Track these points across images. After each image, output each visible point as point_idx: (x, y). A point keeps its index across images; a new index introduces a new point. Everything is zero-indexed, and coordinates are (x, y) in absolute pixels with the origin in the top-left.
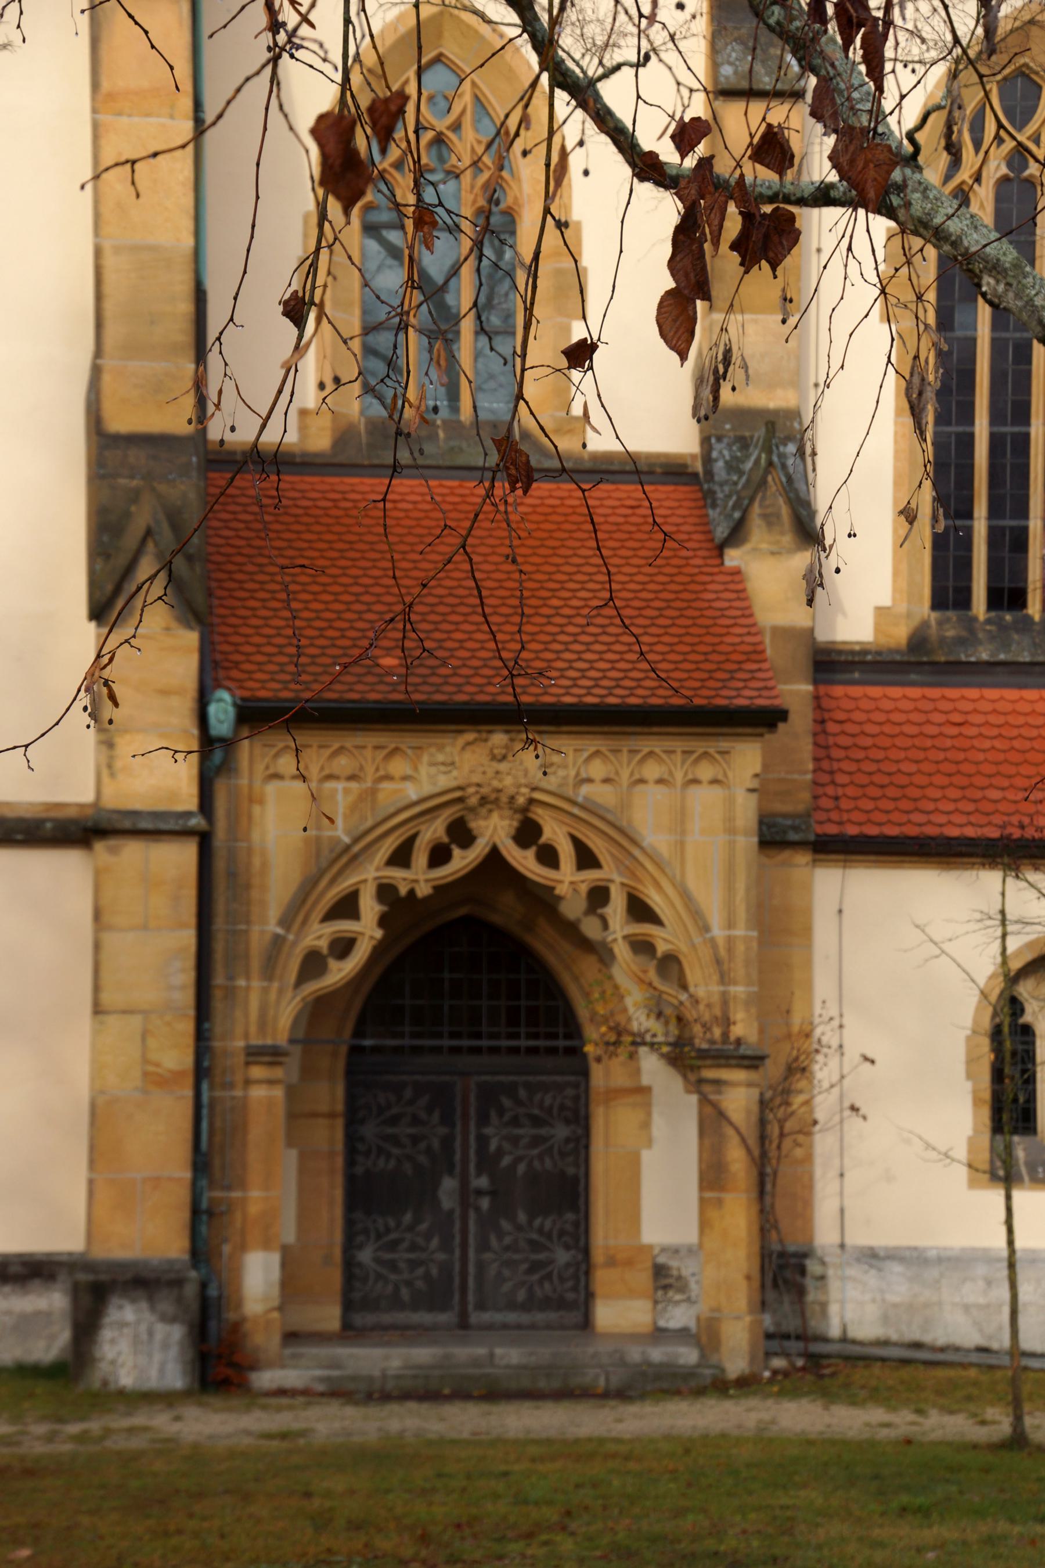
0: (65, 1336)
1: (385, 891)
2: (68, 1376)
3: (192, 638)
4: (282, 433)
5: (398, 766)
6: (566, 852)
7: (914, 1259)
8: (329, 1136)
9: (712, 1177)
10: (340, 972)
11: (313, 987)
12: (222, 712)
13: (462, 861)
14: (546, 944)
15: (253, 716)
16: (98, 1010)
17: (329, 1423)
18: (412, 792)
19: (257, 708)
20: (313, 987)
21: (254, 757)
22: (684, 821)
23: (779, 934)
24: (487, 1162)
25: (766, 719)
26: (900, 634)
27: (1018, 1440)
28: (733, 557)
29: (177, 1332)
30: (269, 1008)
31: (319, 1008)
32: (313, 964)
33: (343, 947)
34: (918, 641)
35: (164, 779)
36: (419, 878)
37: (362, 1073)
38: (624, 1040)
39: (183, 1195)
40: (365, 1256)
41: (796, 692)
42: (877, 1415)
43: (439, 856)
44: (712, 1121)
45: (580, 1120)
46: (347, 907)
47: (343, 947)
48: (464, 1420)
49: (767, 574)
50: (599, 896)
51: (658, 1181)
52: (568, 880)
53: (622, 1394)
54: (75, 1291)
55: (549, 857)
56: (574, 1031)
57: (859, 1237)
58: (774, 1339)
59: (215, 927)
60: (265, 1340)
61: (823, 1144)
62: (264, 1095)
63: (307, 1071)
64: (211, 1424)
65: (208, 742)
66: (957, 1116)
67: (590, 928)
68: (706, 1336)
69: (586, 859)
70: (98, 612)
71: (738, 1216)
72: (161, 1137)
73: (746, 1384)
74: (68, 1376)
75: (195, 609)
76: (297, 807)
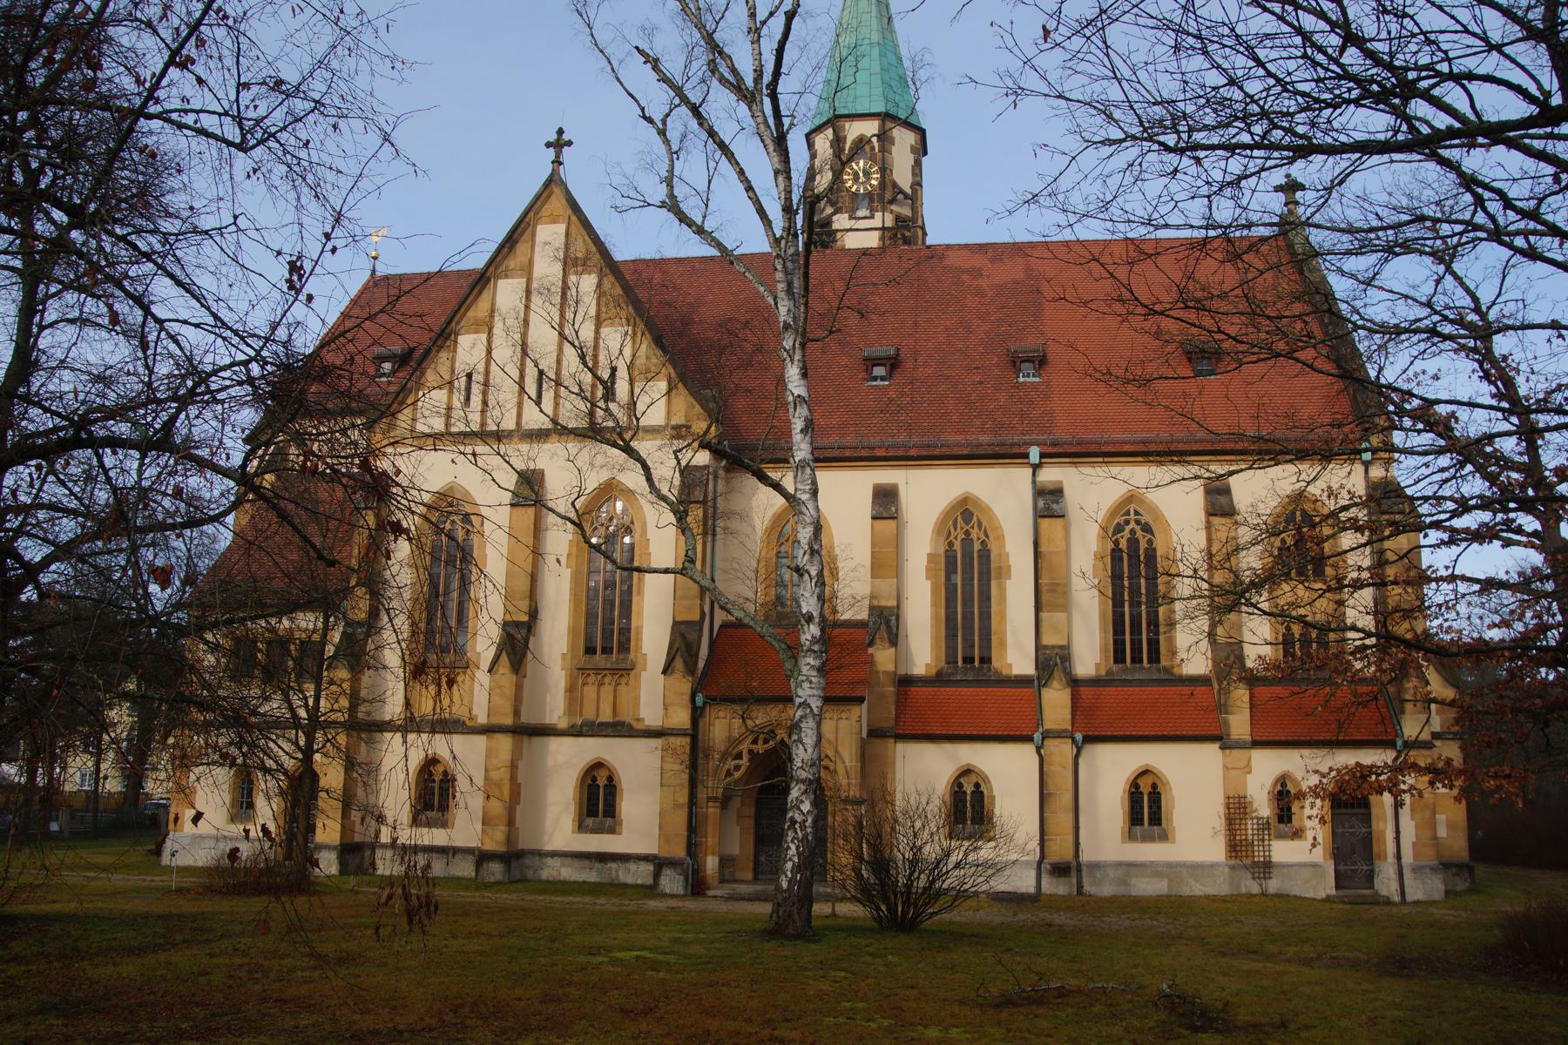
1: (750, 752)
2: (652, 890)
10: (737, 775)
12: (700, 699)
26: (933, 672)
28: (870, 650)
29: (682, 878)
33: (737, 768)
34: (939, 674)
35: (681, 718)
36: (760, 748)
39: (684, 839)
43: (766, 741)
47: (737, 768)
49: (883, 657)
64: (691, 905)
70: (664, 672)
72: (681, 818)
76: (722, 726)
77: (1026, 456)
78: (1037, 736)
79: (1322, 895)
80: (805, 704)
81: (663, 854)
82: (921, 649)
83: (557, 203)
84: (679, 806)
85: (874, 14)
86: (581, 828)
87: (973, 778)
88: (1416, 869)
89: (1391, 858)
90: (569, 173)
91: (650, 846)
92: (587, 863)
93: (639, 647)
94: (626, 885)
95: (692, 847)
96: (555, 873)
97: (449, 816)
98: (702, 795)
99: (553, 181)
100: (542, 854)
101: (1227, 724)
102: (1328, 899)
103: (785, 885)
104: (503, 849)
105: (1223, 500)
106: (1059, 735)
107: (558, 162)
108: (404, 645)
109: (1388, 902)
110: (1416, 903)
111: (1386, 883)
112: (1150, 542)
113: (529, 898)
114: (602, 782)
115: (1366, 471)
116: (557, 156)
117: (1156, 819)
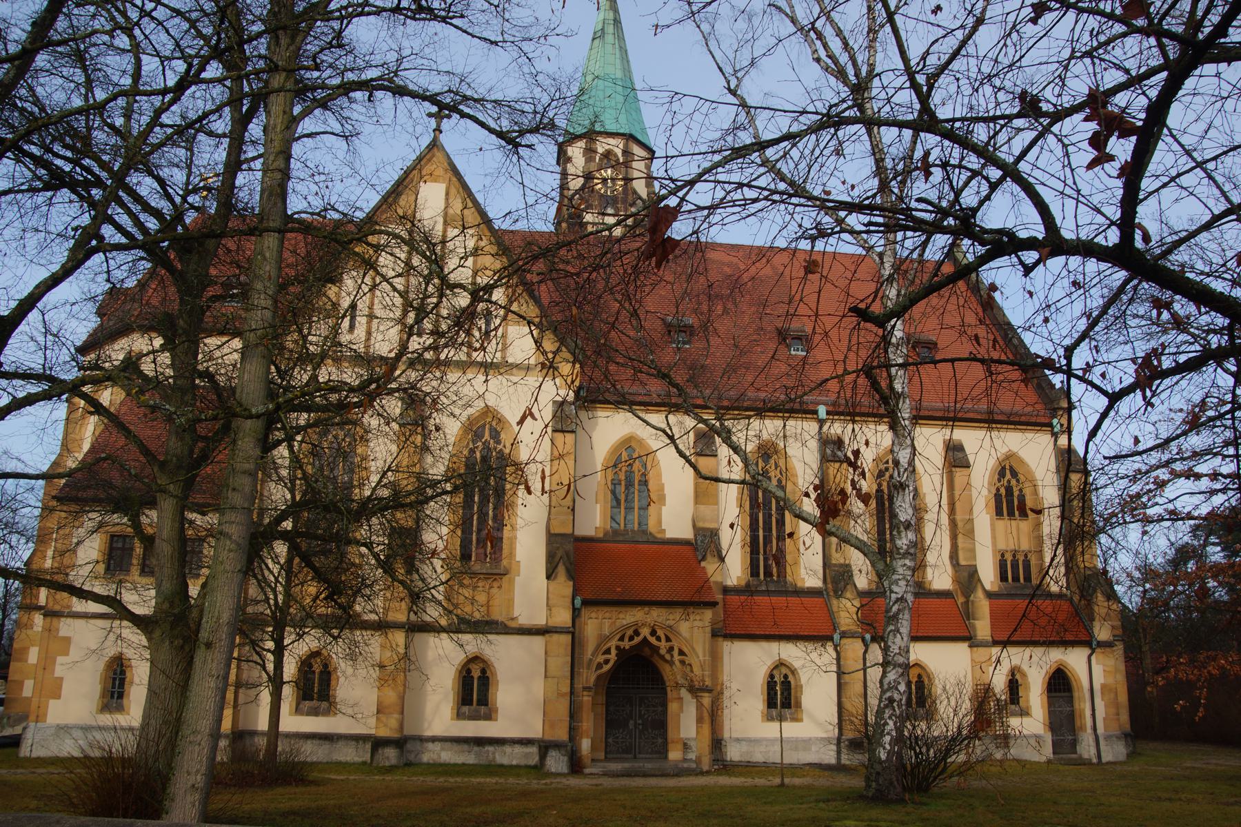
0: (537, 758)
1: (618, 648)
2: (538, 769)
3: (571, 583)
4: (590, 532)
5: (621, 616)
6: (663, 638)
7: (750, 741)
8: (602, 710)
9: (700, 720)
10: (606, 668)
11: (599, 672)
12: (578, 601)
13: (637, 640)
14: (656, 660)
15: (585, 603)
16: (546, 677)
17: (607, 782)
18: (625, 622)
19: (588, 599)
20: (599, 672)
21: (585, 613)
22: (692, 631)
23: (715, 658)
24: (641, 717)
25: (713, 604)
26: (743, 583)
27: (782, 785)
28: (703, 564)
29: (566, 758)
30: (588, 677)
31: (599, 678)
32: (599, 666)
33: (607, 662)
34: (748, 585)
35: (563, 617)
36: (626, 644)
37: (609, 694)
38: (678, 686)
40: (610, 740)
41: (719, 597)
42: (743, 779)
43: (631, 638)
44: (700, 706)
45: (664, 705)
46: (608, 651)
47: (607, 662)
48: (639, 782)
49: (710, 566)
50: (671, 649)
51: (686, 722)
52: (663, 645)
53: (677, 775)
54: (540, 747)
55: (659, 639)
56: (663, 682)
57: (735, 735)
58: (715, 761)
59: (538, 688)
60: (587, 761)
61: (726, 712)
62: (586, 699)
63: (596, 693)
64: (574, 782)
65: (574, 609)
66: (758, 703)
67: (668, 657)
68: (698, 761)
69: (668, 639)
70: (548, 577)
71: (706, 729)
72: (563, 707)
73: (708, 773)
74: (538, 769)
75: (571, 576)
76: (596, 625)
77: (816, 412)
78: (836, 637)
79: (1043, 759)
80: (901, 600)
81: (547, 738)
82: (734, 567)
83: (436, 165)
84: (563, 695)
85: (618, 55)
86: (459, 716)
87: (784, 670)
88: (1107, 738)
89: (1089, 730)
90: (443, 138)
91: (535, 730)
92: (466, 747)
93: (512, 554)
94: (502, 766)
95: (573, 731)
96: (435, 757)
97: (125, 701)
99: (434, 145)
100: (422, 740)
101: (974, 627)
102: (1049, 762)
103: (883, 756)
104: (396, 735)
105: (960, 455)
106: (853, 635)
107: (438, 130)
108: (1227, 504)
109: (1088, 763)
110: (1108, 763)
111: (1087, 749)
112: (1021, 490)
113: (452, 780)
114: (476, 673)
115: (1056, 441)
116: (439, 125)
117: (787, 704)
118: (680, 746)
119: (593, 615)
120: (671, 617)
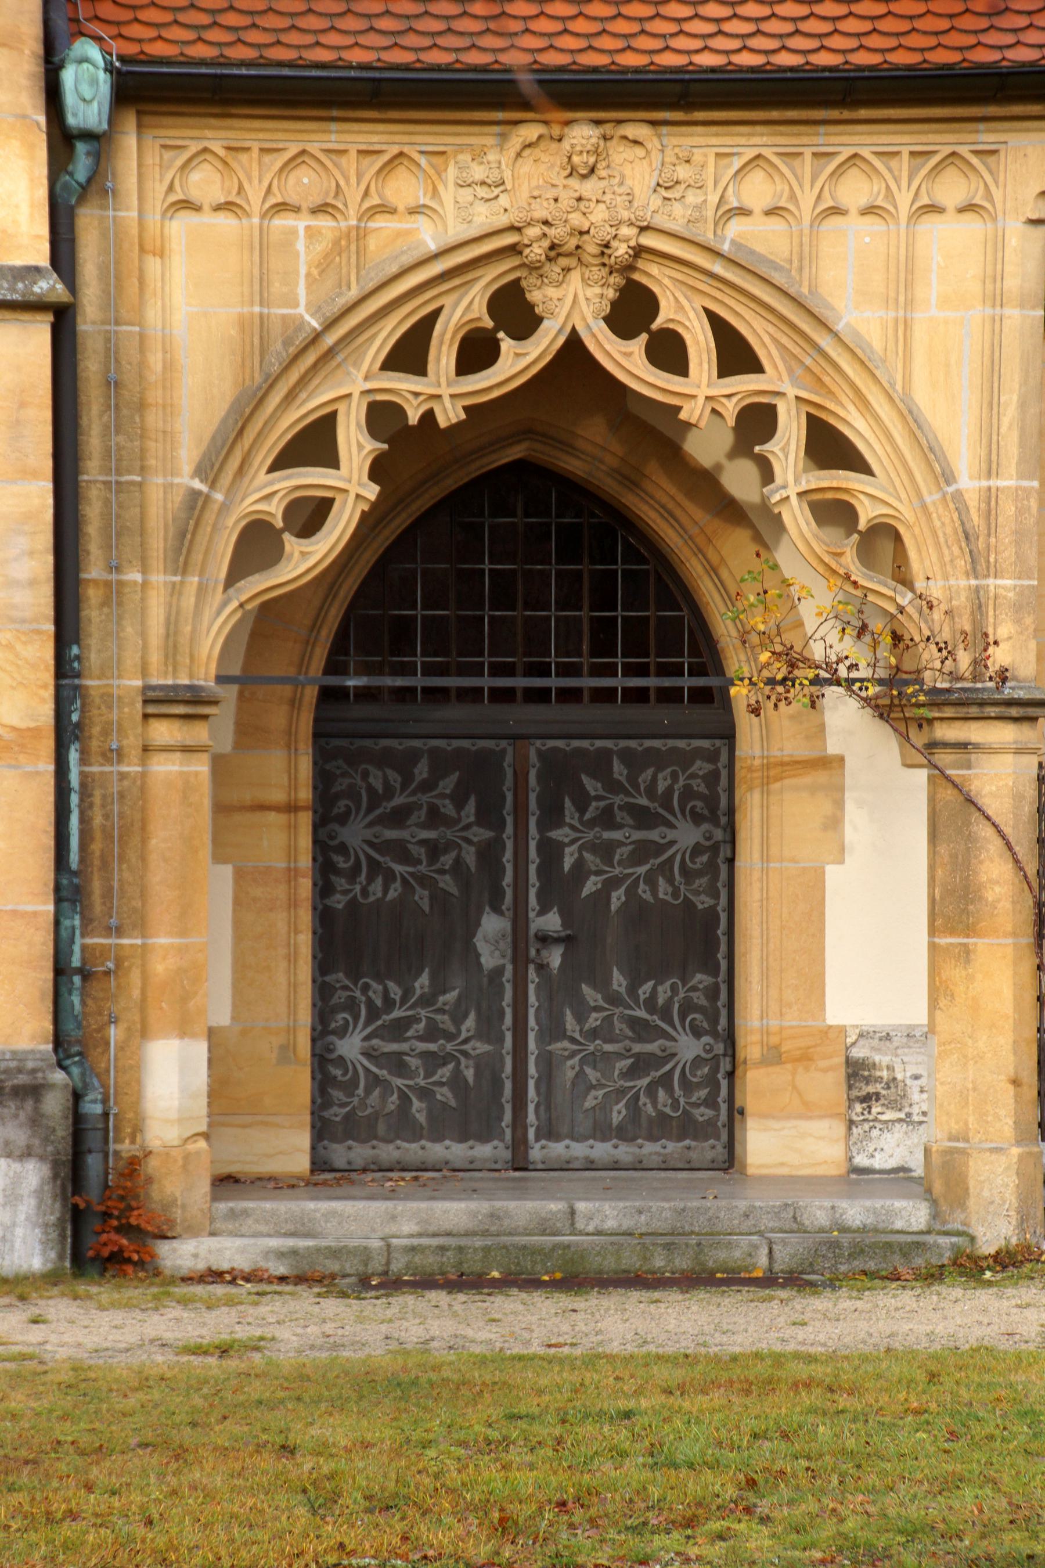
1: (382, 416)
5: (403, 189)
8: (287, 845)
9: (952, 910)
10: (306, 558)
11: (257, 585)
13: (518, 361)
18: (428, 236)
20: (257, 585)
24: (558, 888)
30: (180, 619)
31: (267, 620)
32: (257, 545)
33: (310, 515)
36: (443, 393)
37: (338, 732)
38: (798, 676)
40: (350, 1047)
43: (477, 352)
44: (954, 813)
46: (315, 444)
47: (310, 515)
48: (530, 1322)
50: (757, 422)
52: (702, 393)
55: (669, 352)
56: (706, 655)
60: (179, 1186)
62: (173, 774)
63: (248, 733)
64: (96, 1330)
65: (62, 138)
67: (739, 481)
69: (735, 355)
86: (775, 406)
98: (121, 674)
118: (827, 1083)
119: (205, 183)
120: (757, 190)
